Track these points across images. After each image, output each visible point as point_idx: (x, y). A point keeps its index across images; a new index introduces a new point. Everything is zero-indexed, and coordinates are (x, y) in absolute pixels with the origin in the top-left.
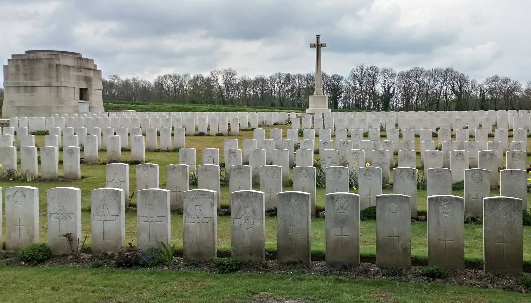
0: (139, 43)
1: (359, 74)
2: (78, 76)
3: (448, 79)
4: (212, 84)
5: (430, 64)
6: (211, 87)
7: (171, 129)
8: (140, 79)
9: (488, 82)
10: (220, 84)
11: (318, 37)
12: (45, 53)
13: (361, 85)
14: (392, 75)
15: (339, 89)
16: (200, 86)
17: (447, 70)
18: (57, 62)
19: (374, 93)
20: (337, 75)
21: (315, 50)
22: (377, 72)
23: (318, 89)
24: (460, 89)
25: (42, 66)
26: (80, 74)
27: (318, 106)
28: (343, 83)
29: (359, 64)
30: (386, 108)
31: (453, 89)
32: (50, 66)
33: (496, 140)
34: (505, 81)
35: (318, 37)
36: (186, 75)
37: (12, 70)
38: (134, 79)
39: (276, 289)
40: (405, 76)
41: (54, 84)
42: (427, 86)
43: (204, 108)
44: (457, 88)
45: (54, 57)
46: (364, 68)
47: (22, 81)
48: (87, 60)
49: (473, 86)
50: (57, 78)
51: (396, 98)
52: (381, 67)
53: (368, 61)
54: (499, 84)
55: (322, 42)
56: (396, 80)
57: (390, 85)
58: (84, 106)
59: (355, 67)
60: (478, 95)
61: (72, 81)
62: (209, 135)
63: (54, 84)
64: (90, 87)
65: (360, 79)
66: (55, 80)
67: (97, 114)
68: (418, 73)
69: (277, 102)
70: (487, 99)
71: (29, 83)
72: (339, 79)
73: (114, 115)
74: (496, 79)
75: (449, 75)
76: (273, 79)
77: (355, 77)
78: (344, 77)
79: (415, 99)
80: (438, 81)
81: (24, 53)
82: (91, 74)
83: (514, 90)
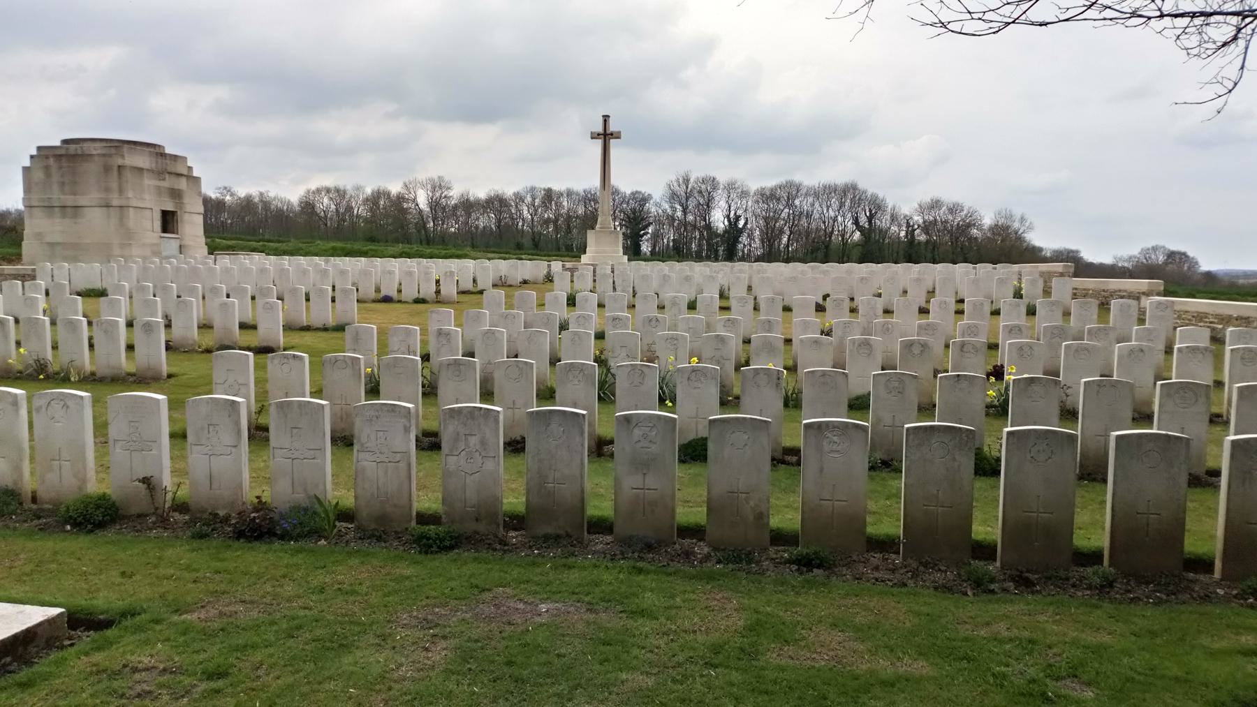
1: (681, 191)
4: (405, 205)
6: (405, 212)
7: (330, 289)
8: (272, 194)
9: (922, 209)
10: (421, 206)
11: (606, 119)
12: (98, 145)
13: (685, 211)
14: (744, 194)
15: (643, 219)
17: (846, 185)
18: (120, 162)
19: (708, 227)
21: (599, 142)
22: (715, 188)
23: (605, 219)
24: (870, 222)
27: (603, 249)
28: (651, 208)
29: (682, 172)
31: (856, 222)
32: (107, 169)
34: (953, 210)
35: (606, 119)
37: (38, 175)
38: (261, 194)
39: (524, 583)
40: (768, 196)
41: (115, 203)
42: (809, 216)
43: (391, 250)
44: (863, 220)
45: (113, 151)
47: (57, 196)
48: (175, 158)
49: (894, 218)
51: (751, 237)
52: (723, 178)
53: (699, 167)
54: (942, 214)
55: (612, 128)
57: (739, 212)
58: (170, 244)
59: (674, 178)
60: (903, 234)
61: (147, 197)
62: (400, 301)
63: (115, 203)
64: (181, 209)
65: (684, 201)
66: (116, 195)
68: (791, 191)
69: (527, 241)
70: (919, 243)
71: (69, 200)
72: (644, 200)
73: (225, 260)
74: (936, 204)
75: (850, 196)
76: (519, 198)
77: (673, 196)
81: (58, 143)
82: (182, 184)
83: (969, 225)
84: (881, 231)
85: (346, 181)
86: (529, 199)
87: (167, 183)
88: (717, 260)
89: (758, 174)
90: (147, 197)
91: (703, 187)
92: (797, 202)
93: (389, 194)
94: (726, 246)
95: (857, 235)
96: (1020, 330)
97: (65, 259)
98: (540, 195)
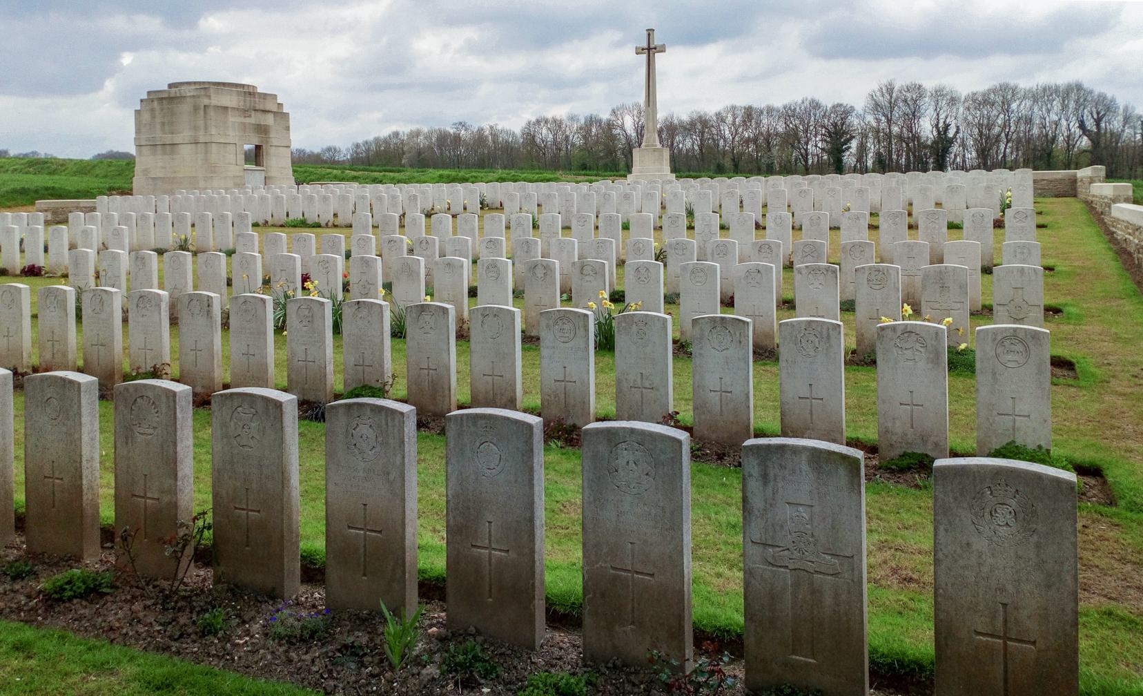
0: (517, 63)
1: (884, 101)
2: (244, 124)
3: (1072, 105)
4: (615, 132)
5: (1033, 75)
6: (613, 138)
7: (593, 216)
8: (499, 127)
10: (629, 132)
11: (650, 33)
12: (193, 87)
13: (889, 121)
14: (953, 101)
15: (845, 133)
18: (206, 101)
19: (916, 137)
21: (644, 57)
22: (921, 96)
23: (652, 138)
24: (1098, 125)
25: (185, 108)
26: (248, 120)
27: (651, 168)
28: (854, 121)
29: (885, 81)
30: (941, 166)
31: (1082, 125)
33: (770, 236)
35: (650, 33)
37: (146, 117)
38: (491, 127)
40: (981, 101)
42: (1029, 121)
43: (492, 176)
44: (1090, 124)
45: (202, 92)
48: (265, 96)
50: (206, 128)
52: (929, 85)
55: (657, 42)
56: (961, 110)
58: (255, 177)
59: (876, 87)
62: (335, 226)
66: (202, 133)
67: (281, 188)
68: (1004, 96)
69: (727, 163)
71: (168, 139)
72: (847, 112)
73: (307, 188)
75: (1073, 96)
76: (721, 118)
77: (877, 106)
78: (856, 107)
79: (1002, 146)
81: (166, 88)
84: (1112, 134)
85: (559, 112)
86: (730, 119)
87: (254, 119)
88: (925, 170)
89: (968, 79)
90: (231, 133)
91: (908, 95)
92: (1014, 106)
93: (600, 121)
94: (937, 155)
95: (1085, 142)
96: (770, 248)
97: (165, 192)
98: (740, 114)
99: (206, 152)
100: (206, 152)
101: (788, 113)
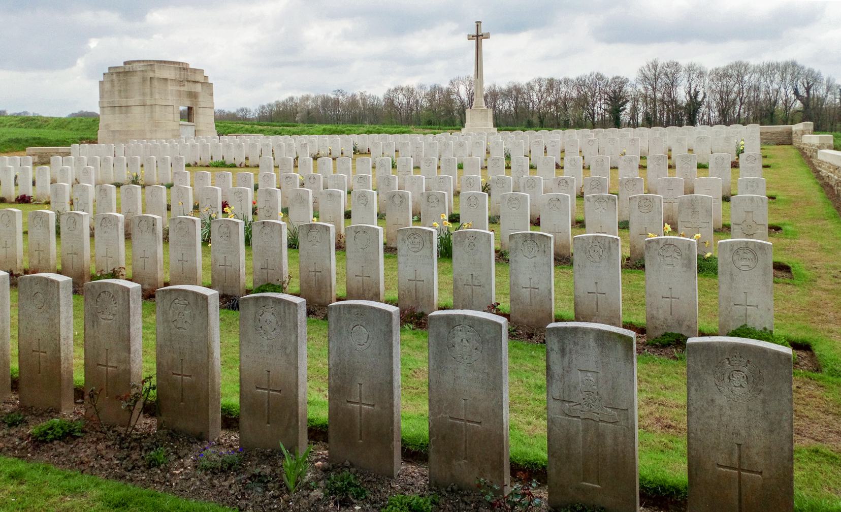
0: (381, 46)
1: (650, 74)
2: (180, 91)
3: (789, 77)
5: (760, 55)
6: (451, 102)
7: (437, 159)
8: (367, 94)
10: (463, 97)
11: (478, 24)
12: (142, 64)
13: (654, 89)
14: (701, 74)
15: (622, 98)
16: (439, 100)
18: (152, 75)
19: (674, 101)
20: (618, 77)
21: (474, 42)
23: (479, 101)
24: (808, 92)
25: (136, 79)
26: (182, 88)
27: (479, 123)
28: (628, 89)
29: (651, 60)
30: (692, 122)
31: (796, 92)
32: (144, 80)
33: (566, 174)
35: (478, 24)
36: (421, 87)
37: (108, 86)
38: (362, 94)
40: (722, 75)
42: (757, 89)
43: (362, 129)
44: (802, 92)
45: (149, 68)
46: (659, 66)
47: (118, 100)
50: (151, 94)
52: (684, 62)
55: (483, 31)
56: (707, 81)
58: (188, 130)
59: (645, 64)
61: (170, 97)
62: (247, 166)
66: (148, 98)
67: (206, 138)
68: (738, 71)
69: (535, 120)
71: (124, 102)
72: (623, 83)
73: (226, 139)
75: (790, 71)
76: (530, 87)
79: (737, 108)
80: (772, 82)
81: (122, 65)
82: (198, 88)
84: (818, 98)
85: (412, 82)
87: (187, 87)
89: (712, 58)
90: (170, 97)
91: (668, 70)
92: (746, 78)
93: (442, 89)
95: (798, 105)
96: (566, 182)
97: (122, 141)
98: (545, 84)
99: (152, 112)
100: (152, 112)
101: (580, 84)
